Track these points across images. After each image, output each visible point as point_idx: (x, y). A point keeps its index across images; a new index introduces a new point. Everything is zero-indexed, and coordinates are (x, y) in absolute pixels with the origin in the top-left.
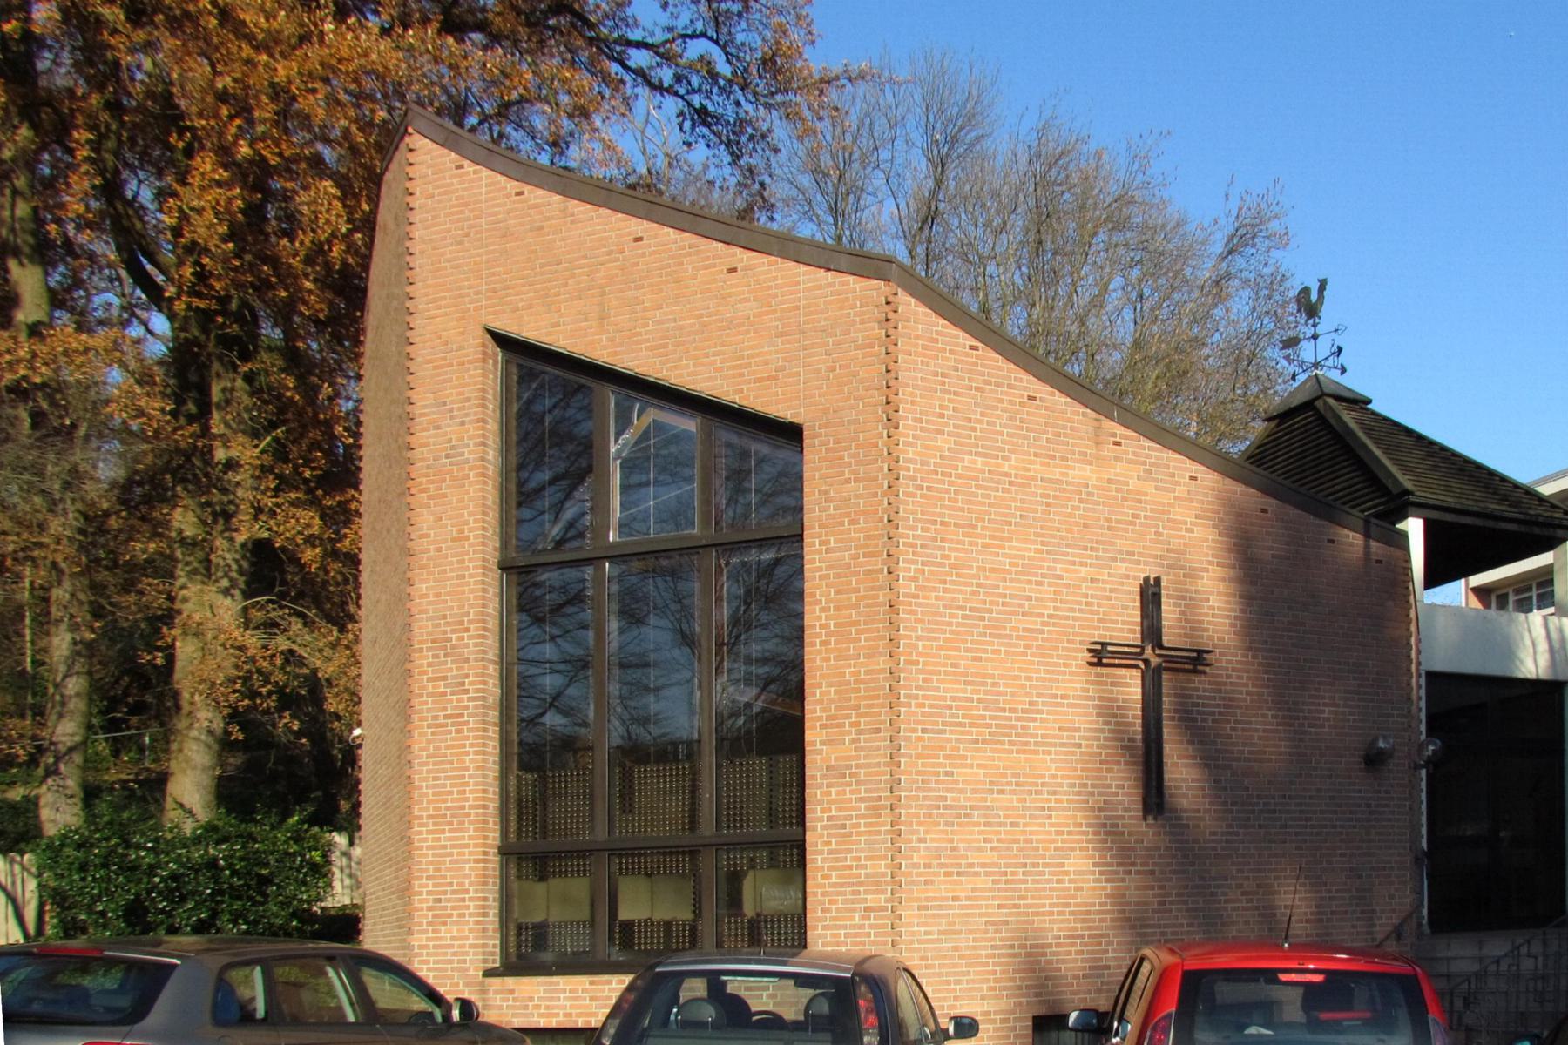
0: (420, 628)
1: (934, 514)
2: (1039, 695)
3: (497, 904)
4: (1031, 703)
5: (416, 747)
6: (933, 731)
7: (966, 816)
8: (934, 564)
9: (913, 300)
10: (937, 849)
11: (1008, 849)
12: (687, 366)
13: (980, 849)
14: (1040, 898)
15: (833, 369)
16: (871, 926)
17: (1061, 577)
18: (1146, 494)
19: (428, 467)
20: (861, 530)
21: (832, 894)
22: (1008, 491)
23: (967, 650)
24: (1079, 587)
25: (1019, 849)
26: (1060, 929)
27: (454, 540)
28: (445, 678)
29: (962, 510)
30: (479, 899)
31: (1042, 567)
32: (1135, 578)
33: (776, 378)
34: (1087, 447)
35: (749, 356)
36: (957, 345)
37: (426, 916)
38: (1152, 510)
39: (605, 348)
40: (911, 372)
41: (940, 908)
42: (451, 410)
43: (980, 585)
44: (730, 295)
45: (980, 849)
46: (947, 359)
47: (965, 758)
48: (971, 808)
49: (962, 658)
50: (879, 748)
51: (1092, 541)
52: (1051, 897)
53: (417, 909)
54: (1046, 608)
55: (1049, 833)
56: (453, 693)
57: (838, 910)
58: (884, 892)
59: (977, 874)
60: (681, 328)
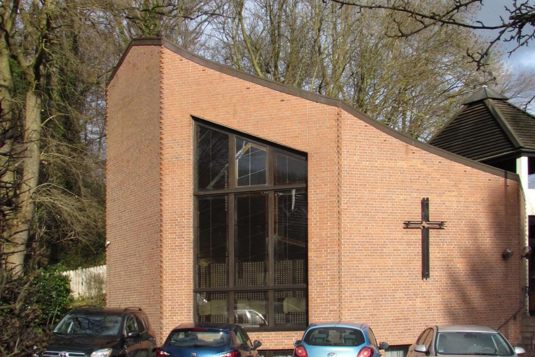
0: (166, 216)
1: (352, 182)
2: (387, 239)
3: (192, 309)
4: (384, 242)
5: (164, 256)
6: (352, 253)
7: (363, 280)
8: (352, 198)
9: (346, 113)
10: (353, 291)
11: (377, 290)
12: (266, 132)
13: (367, 291)
14: (387, 306)
15: (319, 135)
16: (332, 316)
17: (394, 200)
18: (423, 169)
19: (169, 161)
20: (328, 188)
21: (317, 306)
22: (377, 172)
23: (363, 226)
24: (400, 202)
25: (380, 290)
26: (394, 317)
27: (178, 186)
28: (175, 233)
29: (362, 180)
30: (188, 307)
31: (388, 197)
32: (420, 198)
33: (298, 137)
34: (403, 155)
35: (288, 129)
36: (361, 126)
37: (168, 313)
38: (425, 174)
39: (235, 124)
40: (346, 136)
41: (354, 310)
42: (178, 142)
43: (367, 204)
44: (282, 109)
45: (367, 291)
46: (357, 131)
47: (362, 261)
48: (365, 277)
49: (362, 228)
50: (334, 259)
51: (405, 187)
52: (390, 306)
53: (165, 311)
54: (389, 210)
55: (390, 285)
56: (178, 238)
57: (320, 311)
58: (336, 305)
59: (366, 299)
60: (264, 119)
